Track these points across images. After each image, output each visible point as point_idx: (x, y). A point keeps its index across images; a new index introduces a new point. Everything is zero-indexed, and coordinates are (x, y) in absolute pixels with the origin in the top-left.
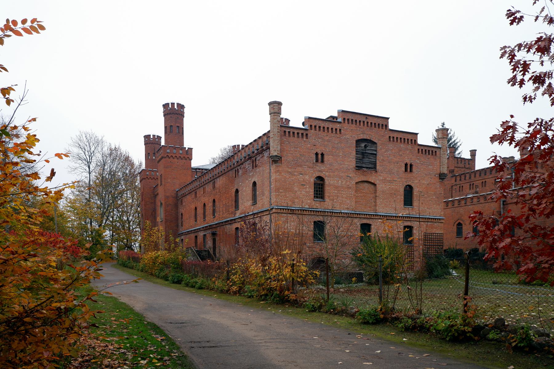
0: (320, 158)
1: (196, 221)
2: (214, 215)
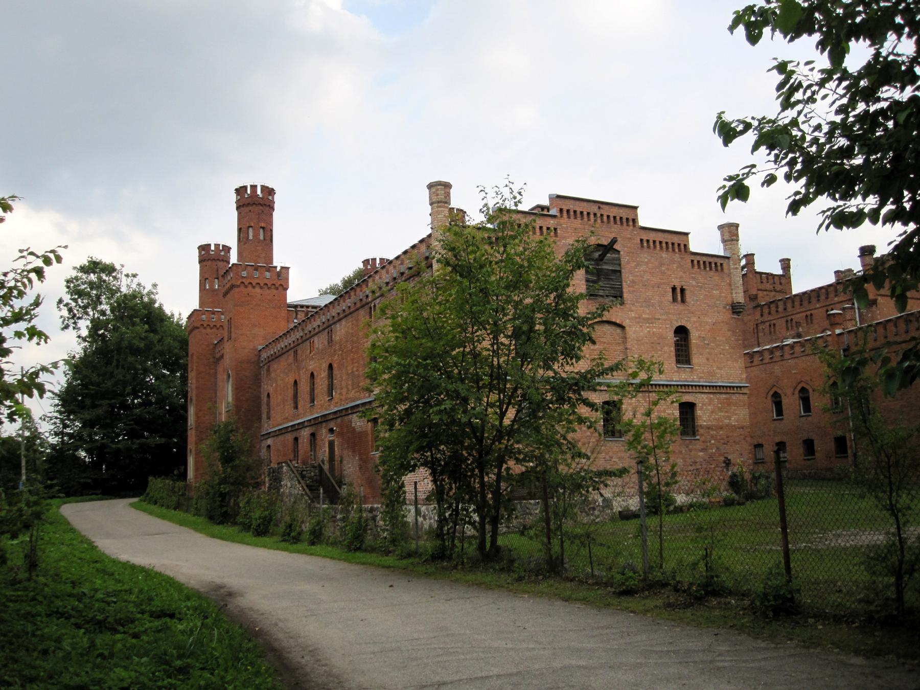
1: (296, 407)
2: (330, 394)
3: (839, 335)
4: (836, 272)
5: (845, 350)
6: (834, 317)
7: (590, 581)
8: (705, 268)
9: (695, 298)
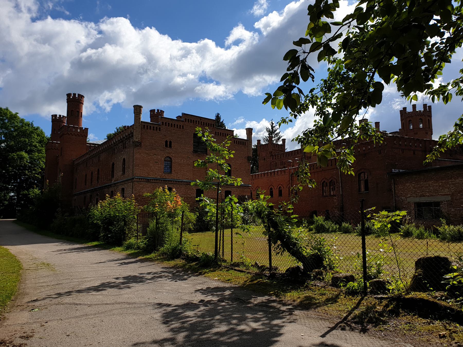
0: (168, 144)
1: (86, 185)
2: (98, 181)
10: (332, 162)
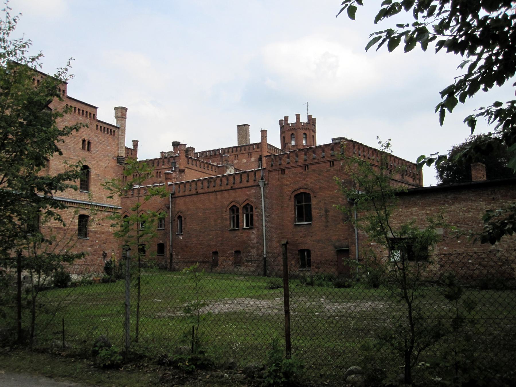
3: (169, 185)
4: (162, 153)
5: (172, 194)
6: (168, 175)
7: (64, 354)
8: (104, 131)
9: (96, 149)
10: (228, 180)
